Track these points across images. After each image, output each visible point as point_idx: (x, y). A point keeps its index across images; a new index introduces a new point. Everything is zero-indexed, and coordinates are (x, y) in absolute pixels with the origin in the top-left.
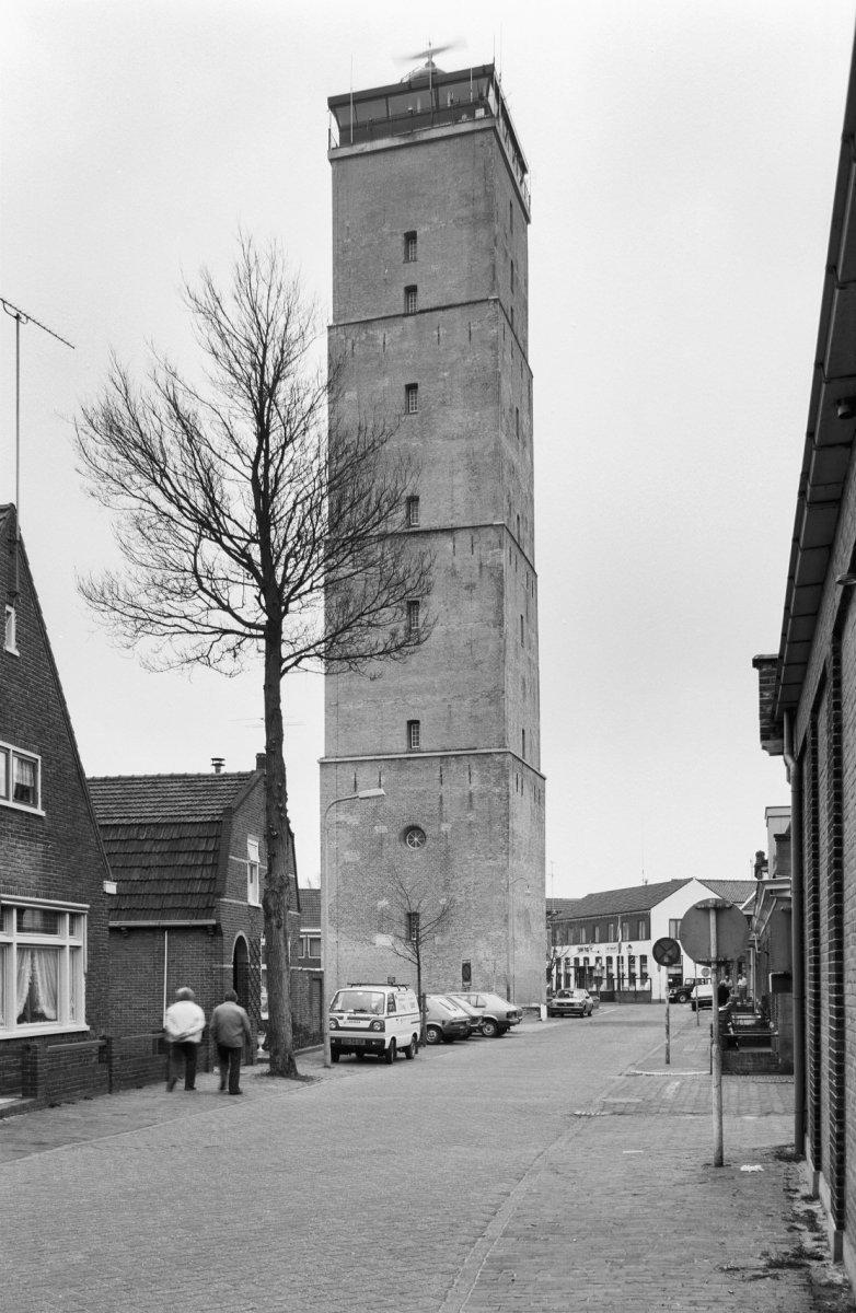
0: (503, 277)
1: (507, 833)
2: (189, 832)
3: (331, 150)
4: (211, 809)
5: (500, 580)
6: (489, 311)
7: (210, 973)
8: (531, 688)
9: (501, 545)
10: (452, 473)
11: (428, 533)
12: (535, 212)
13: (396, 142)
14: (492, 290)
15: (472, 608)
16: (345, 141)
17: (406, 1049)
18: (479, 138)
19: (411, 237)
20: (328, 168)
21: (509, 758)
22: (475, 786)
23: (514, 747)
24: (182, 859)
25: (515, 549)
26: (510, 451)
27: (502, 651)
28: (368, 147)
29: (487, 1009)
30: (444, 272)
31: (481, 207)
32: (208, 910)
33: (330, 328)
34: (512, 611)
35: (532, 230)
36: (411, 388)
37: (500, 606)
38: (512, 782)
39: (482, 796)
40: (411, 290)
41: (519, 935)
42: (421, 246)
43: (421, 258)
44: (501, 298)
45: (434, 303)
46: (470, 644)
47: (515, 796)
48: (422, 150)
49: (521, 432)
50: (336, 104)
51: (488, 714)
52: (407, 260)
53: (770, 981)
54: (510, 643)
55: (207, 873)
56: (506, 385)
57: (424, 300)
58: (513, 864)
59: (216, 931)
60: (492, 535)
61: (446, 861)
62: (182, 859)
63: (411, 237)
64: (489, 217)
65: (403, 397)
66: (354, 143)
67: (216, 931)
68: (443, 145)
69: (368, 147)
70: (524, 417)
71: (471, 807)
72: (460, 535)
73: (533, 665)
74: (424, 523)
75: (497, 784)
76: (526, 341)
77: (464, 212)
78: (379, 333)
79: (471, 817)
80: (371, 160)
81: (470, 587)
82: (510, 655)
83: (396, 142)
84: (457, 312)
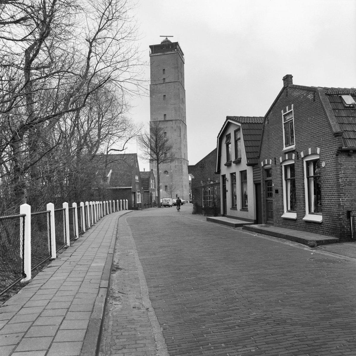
0: (180, 77)
1: (182, 172)
2: (144, 180)
3: (150, 54)
4: (147, 177)
5: (180, 129)
6: (177, 83)
7: (148, 197)
8: (186, 146)
9: (180, 123)
10: (172, 110)
11: (168, 121)
12: (185, 62)
13: (161, 54)
14: (178, 80)
15: (176, 134)
16: (152, 53)
17: (171, 206)
18: (175, 54)
19: (164, 70)
20: (150, 57)
21: (182, 159)
22: (177, 164)
23: (183, 157)
24: (144, 183)
25: (183, 123)
26: (181, 106)
27: (181, 141)
28: (156, 54)
29: (103, 295)
30: (170, 77)
31: (176, 65)
32: (148, 189)
33: (150, 85)
34: (182, 134)
35: (185, 65)
36: (164, 96)
37: (180, 133)
38: (183, 163)
39: (178, 166)
40: (164, 79)
41: (184, 189)
42: (166, 72)
43: (166, 74)
44: (179, 81)
45: (168, 82)
46: (175, 140)
47: (183, 165)
48: (166, 55)
49: (183, 102)
50: (151, 47)
51: (178, 152)
52: (163, 74)
53: (100, 201)
54: (182, 139)
55: (147, 185)
56: (181, 95)
57: (167, 81)
58: (183, 177)
59: (149, 192)
60: (179, 121)
61: (172, 177)
62: (144, 183)
63: (164, 70)
64: (178, 67)
65: (163, 97)
66: (154, 54)
67: (149, 192)
68: (169, 55)
69: (156, 54)
70: (184, 99)
71: (176, 168)
72: (173, 121)
73: (186, 142)
74: (167, 119)
75: (180, 164)
76: (184, 85)
77: (173, 66)
78: (159, 86)
79: (176, 169)
80: (157, 56)
81: (175, 130)
82: (182, 141)
83: (161, 54)
84: (172, 83)
